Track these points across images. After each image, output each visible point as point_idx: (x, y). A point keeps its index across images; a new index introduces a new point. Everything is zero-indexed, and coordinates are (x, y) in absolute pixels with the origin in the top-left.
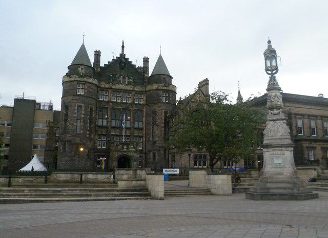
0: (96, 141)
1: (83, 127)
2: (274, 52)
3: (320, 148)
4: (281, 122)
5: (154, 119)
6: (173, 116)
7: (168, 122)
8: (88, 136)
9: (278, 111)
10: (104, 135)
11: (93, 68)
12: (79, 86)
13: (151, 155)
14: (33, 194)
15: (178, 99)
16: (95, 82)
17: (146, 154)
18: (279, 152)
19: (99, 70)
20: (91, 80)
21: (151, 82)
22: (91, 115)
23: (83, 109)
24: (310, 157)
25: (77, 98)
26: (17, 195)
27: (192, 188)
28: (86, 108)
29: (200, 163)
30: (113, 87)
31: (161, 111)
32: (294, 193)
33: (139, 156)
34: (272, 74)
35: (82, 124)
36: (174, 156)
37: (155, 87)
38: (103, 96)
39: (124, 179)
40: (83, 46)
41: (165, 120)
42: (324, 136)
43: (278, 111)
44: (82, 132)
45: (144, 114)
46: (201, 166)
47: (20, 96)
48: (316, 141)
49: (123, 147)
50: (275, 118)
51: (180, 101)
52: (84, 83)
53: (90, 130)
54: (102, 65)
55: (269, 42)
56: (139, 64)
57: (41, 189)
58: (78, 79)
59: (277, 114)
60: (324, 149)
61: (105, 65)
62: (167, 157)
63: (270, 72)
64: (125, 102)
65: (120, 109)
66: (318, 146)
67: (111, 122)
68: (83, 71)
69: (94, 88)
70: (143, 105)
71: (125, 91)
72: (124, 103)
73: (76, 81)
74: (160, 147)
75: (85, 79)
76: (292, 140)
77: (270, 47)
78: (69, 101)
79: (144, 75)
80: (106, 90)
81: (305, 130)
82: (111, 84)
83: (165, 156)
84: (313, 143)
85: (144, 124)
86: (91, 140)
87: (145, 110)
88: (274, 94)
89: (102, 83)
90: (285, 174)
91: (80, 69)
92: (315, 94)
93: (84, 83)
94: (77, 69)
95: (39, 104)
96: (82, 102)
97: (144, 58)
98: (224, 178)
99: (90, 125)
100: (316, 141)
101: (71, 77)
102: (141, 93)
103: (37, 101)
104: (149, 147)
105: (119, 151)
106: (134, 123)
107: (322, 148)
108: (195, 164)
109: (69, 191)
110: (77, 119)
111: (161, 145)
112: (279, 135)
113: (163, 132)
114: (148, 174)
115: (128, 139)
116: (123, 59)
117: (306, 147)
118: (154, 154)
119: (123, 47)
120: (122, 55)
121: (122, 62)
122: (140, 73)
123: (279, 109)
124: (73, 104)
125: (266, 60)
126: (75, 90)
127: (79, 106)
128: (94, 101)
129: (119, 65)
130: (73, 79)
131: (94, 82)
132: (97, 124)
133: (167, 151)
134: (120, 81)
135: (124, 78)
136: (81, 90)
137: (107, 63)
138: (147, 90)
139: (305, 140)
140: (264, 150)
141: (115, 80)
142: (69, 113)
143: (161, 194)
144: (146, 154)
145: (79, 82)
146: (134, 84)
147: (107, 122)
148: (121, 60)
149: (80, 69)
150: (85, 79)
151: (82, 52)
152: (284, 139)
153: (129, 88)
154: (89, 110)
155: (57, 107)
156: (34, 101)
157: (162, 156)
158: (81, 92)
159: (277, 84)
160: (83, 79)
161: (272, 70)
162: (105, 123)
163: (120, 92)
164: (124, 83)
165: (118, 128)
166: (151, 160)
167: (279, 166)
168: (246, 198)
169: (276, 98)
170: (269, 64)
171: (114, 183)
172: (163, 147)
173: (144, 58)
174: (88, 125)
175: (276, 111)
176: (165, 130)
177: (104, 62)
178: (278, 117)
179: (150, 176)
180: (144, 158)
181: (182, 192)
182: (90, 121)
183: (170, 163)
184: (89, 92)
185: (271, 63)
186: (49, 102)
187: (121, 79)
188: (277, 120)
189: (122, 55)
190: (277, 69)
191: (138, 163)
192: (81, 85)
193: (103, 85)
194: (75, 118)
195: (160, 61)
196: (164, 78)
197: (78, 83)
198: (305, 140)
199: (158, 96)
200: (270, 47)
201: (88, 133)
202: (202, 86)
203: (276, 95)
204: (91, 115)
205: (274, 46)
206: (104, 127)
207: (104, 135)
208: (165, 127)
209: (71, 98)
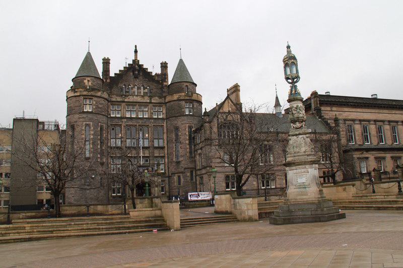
1: (92, 150)
2: (294, 58)
3: (374, 159)
5: (177, 135)
6: (198, 130)
7: (194, 138)
9: (301, 125)
11: (102, 80)
12: (86, 102)
13: (176, 178)
14: (35, 230)
15: (203, 111)
16: (105, 95)
17: (169, 177)
18: (303, 170)
19: (108, 81)
20: (99, 94)
21: (169, 90)
22: (101, 135)
23: (92, 128)
24: (362, 169)
25: (84, 115)
26: (18, 233)
28: (95, 127)
29: (233, 184)
30: (126, 100)
31: (185, 126)
32: (322, 214)
33: (160, 180)
34: (293, 83)
35: (91, 146)
36: (202, 178)
37: (176, 97)
38: (114, 111)
39: (141, 211)
40: (89, 54)
41: (190, 136)
42: (393, 143)
43: (301, 125)
45: (165, 131)
46: (229, 188)
47: (20, 116)
48: (368, 150)
50: (297, 133)
51: (205, 112)
53: (102, 153)
54: (112, 74)
55: (288, 47)
56: (156, 70)
57: (44, 224)
58: (85, 93)
60: (395, 159)
61: (115, 74)
62: (194, 180)
63: (290, 81)
65: (136, 125)
66: (371, 156)
67: (126, 141)
68: (90, 83)
69: (103, 102)
70: (163, 119)
71: (141, 104)
72: (140, 118)
73: (83, 95)
74: (185, 169)
77: (289, 52)
78: (75, 120)
79: (162, 84)
81: (357, 138)
83: (192, 179)
84: (365, 153)
85: (166, 142)
86: (102, 164)
87: (165, 125)
88: (295, 106)
90: (309, 194)
91: (86, 81)
92: (367, 95)
95: (43, 123)
96: (90, 120)
97: (161, 64)
98: (249, 202)
99: (101, 147)
100: (368, 150)
101: (76, 92)
102: (160, 104)
103: (40, 120)
104: (172, 169)
106: (153, 141)
107: (376, 158)
108: (227, 187)
109: (75, 226)
110: (86, 141)
111: (186, 166)
113: (188, 150)
114: (163, 202)
115: (147, 161)
117: (358, 158)
118: (179, 177)
119: (136, 52)
120: (136, 61)
121: (135, 70)
122: (158, 82)
123: (302, 122)
124: (79, 123)
125: (285, 67)
129: (132, 74)
130: (78, 94)
131: (103, 96)
133: (194, 172)
134: (134, 92)
135: (139, 88)
136: (88, 106)
137: (123, 69)
138: (167, 101)
139: (357, 150)
140: (287, 168)
141: (128, 92)
142: (76, 134)
143: (177, 224)
144: (169, 177)
147: (121, 141)
151: (88, 61)
153: (147, 100)
154: (99, 129)
155: (63, 126)
156: (37, 120)
157: (189, 179)
158: (88, 109)
159: (299, 94)
161: (293, 79)
162: (119, 143)
163: (135, 105)
165: (134, 148)
166: (176, 184)
167: (303, 186)
168: (270, 223)
169: (298, 110)
170: (288, 73)
171: (125, 214)
172: (188, 168)
173: (161, 64)
174: (99, 147)
175: (298, 125)
176: (190, 148)
177: (114, 70)
178: (301, 131)
179: (165, 204)
180: (167, 182)
182: (101, 142)
183: (198, 187)
184: (97, 107)
185: (291, 71)
186: (54, 121)
187: (135, 89)
189: (136, 61)
190: (298, 77)
191: (160, 189)
195: (181, 67)
196: (187, 86)
198: (357, 150)
199: (181, 107)
200: (289, 52)
202: (232, 93)
203: (297, 106)
205: (294, 52)
207: (119, 158)
208: (190, 144)
209: (77, 116)
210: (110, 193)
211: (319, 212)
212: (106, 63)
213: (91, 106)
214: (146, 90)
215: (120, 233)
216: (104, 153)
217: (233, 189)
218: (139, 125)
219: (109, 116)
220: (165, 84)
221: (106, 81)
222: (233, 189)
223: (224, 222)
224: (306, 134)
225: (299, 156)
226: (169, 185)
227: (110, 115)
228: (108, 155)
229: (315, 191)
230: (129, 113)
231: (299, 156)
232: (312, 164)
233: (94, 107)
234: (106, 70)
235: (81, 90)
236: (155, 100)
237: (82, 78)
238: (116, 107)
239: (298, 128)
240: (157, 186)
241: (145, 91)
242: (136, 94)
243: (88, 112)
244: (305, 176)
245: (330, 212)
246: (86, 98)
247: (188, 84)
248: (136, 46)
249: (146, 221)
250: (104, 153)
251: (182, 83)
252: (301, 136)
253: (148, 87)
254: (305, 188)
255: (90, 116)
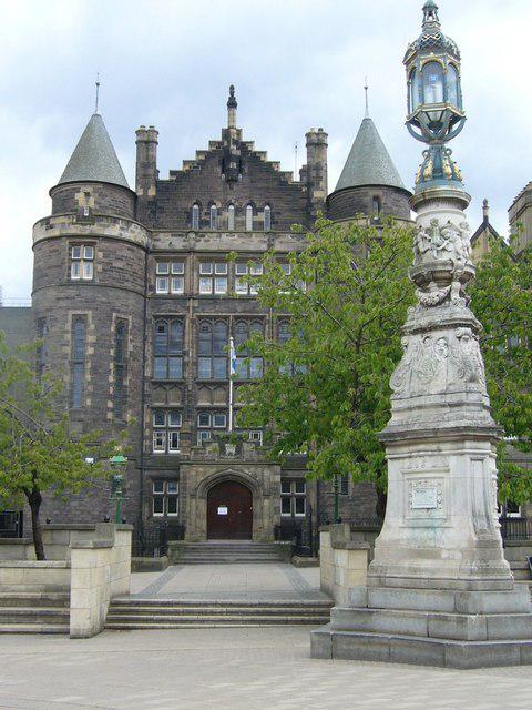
0: (147, 432)
1: (90, 388)
4: (451, 334)
8: (110, 415)
9: (442, 292)
10: (175, 412)
12: (77, 254)
18: (429, 463)
19: (152, 192)
20: (114, 231)
22: (120, 346)
23: (92, 327)
25: (72, 292)
27: (419, 617)
28: (103, 322)
30: (201, 245)
38: (167, 279)
44: (89, 402)
49: (223, 449)
52: (91, 241)
53: (121, 397)
56: (291, 162)
58: (74, 230)
59: (439, 303)
61: (172, 173)
64: (165, 292)
65: (226, 318)
67: (196, 364)
71: (245, 257)
75: (96, 229)
76: (492, 411)
79: (309, 196)
80: (177, 256)
82: (192, 236)
89: (161, 236)
90: (444, 555)
91: (80, 197)
93: (91, 241)
94: (70, 197)
96: (89, 303)
97: (308, 135)
105: (211, 463)
112: (438, 386)
116: (233, 147)
119: (232, 104)
121: (232, 161)
126: (64, 267)
127: (79, 319)
128: (132, 302)
129: (219, 169)
130: (56, 232)
131: (127, 235)
132: (148, 373)
134: (225, 223)
135: (239, 211)
136: (83, 265)
145: (76, 241)
146: (278, 226)
147: (184, 365)
148: (227, 150)
149: (80, 197)
150: (96, 229)
151: (91, 144)
152: (451, 405)
153: (256, 243)
154: (113, 329)
158: (84, 273)
160: (87, 230)
164: (240, 228)
169: (436, 239)
173: (308, 135)
175: (436, 293)
177: (169, 161)
178: (438, 316)
181: (213, 613)
187: (230, 214)
188: (433, 328)
192: (83, 250)
193: (165, 241)
194: (64, 357)
196: (376, 198)
197: (73, 244)
201: (110, 404)
204: (120, 346)
205: (449, 30)
206: (175, 384)
209: (52, 293)
210: (146, 510)
211: (451, 628)
212: (147, 142)
213: (91, 265)
214: (262, 217)
215: (177, 628)
216: (127, 396)
217: (513, 515)
218: (236, 318)
219: (149, 293)
220: (317, 194)
221: (146, 192)
222: (513, 515)
223: (287, 622)
224: (455, 326)
225: (420, 407)
226: (318, 494)
227: (153, 288)
228: (143, 402)
229: (464, 545)
230: (210, 282)
231: (420, 407)
232: (463, 439)
233: (100, 268)
234: (146, 165)
235: (65, 220)
236: (285, 243)
237: (71, 187)
238: (172, 268)
239: (432, 306)
240: (267, 496)
241: (256, 218)
242: (231, 228)
243: (82, 283)
244: (435, 482)
245: (493, 632)
246: (79, 244)
247: (379, 192)
248: (232, 88)
249: (34, 602)
250: (127, 396)
251: (363, 190)
252: (436, 335)
253: (267, 208)
254: (433, 528)
255: (88, 293)
